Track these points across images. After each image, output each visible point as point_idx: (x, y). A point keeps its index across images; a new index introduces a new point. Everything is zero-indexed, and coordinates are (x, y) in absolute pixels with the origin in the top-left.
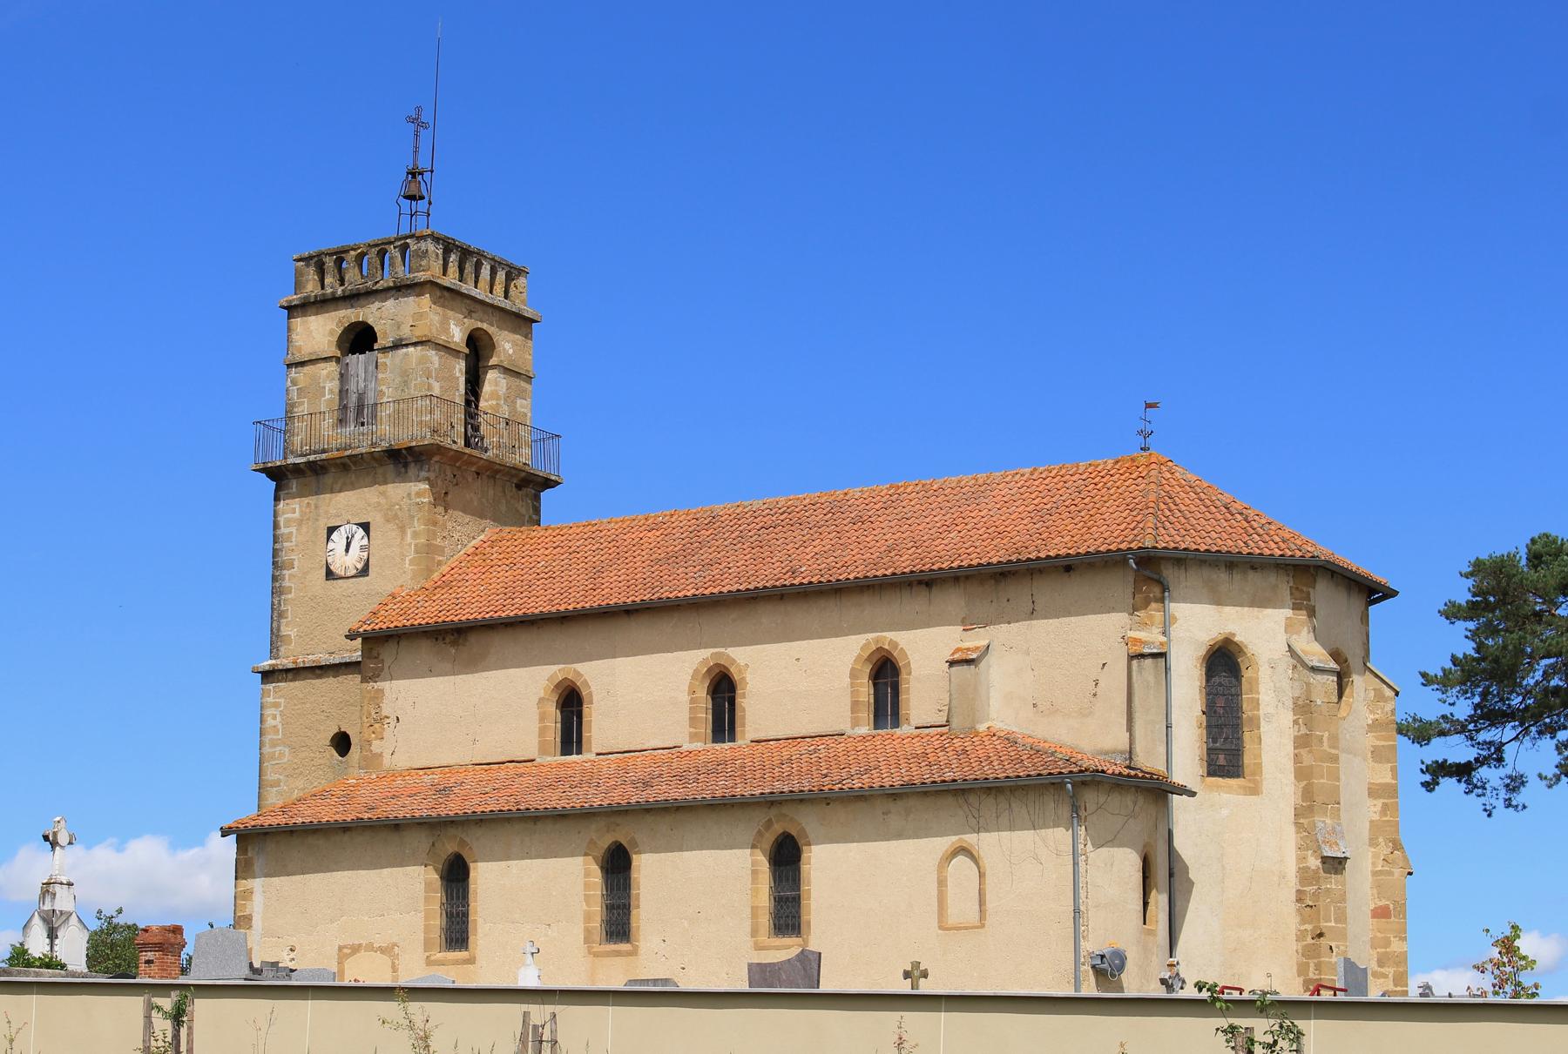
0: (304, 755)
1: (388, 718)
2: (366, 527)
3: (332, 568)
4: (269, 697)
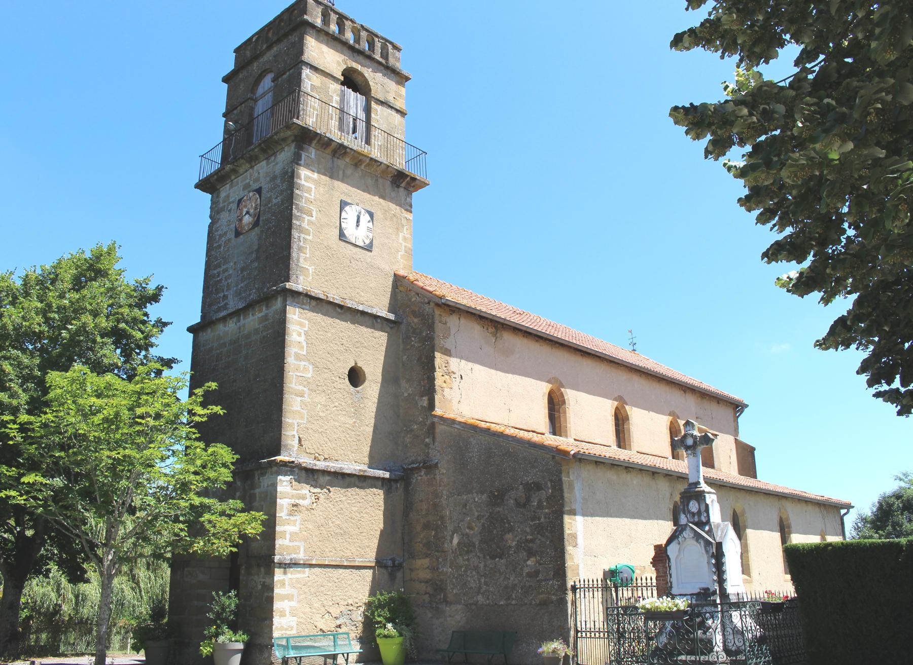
0: (325, 376)
1: (454, 373)
2: (371, 215)
3: (345, 232)
4: (295, 315)
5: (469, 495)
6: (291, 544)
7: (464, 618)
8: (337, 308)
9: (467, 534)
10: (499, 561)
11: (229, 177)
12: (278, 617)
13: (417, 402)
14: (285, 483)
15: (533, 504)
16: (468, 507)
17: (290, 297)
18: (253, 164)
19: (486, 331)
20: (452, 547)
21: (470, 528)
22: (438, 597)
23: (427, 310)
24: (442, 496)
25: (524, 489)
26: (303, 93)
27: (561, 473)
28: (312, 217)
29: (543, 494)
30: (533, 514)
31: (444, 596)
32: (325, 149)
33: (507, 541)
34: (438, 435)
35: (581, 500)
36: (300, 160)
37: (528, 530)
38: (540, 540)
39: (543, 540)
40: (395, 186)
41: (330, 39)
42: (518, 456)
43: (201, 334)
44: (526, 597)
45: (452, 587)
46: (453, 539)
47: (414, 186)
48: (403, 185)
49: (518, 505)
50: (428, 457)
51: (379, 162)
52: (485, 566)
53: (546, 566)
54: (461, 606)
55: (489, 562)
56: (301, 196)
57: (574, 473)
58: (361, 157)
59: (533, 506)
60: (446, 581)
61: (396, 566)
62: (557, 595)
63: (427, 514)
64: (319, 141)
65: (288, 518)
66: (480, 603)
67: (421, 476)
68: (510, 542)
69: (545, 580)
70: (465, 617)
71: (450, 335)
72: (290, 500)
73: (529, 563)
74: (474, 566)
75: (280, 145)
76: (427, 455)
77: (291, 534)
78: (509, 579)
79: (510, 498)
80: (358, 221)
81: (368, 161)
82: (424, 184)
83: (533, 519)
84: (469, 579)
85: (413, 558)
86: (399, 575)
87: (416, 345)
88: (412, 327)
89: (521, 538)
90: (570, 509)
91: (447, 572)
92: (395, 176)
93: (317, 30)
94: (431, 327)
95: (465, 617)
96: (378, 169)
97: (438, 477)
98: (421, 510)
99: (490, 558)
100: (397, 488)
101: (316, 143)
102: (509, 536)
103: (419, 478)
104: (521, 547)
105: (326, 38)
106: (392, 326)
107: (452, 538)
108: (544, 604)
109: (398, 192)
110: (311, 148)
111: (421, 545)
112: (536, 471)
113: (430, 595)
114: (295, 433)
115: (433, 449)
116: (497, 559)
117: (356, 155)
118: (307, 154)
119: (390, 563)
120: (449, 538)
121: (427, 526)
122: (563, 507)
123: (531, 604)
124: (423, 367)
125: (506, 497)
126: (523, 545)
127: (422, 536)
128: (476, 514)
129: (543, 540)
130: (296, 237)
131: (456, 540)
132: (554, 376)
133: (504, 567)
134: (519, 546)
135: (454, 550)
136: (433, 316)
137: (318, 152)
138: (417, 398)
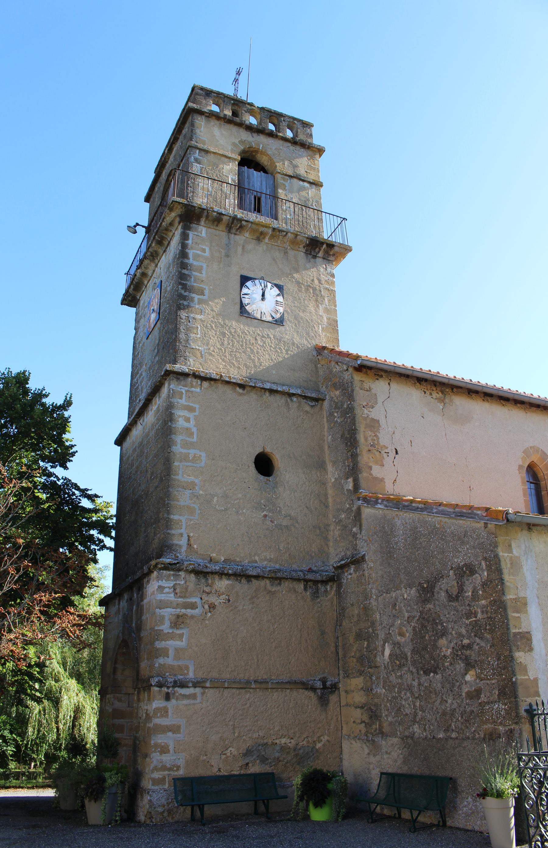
4: (181, 398)
5: (397, 592)
6: (176, 663)
7: (401, 756)
8: (238, 389)
9: (399, 643)
10: (434, 676)
11: (143, 283)
12: (158, 754)
13: (342, 486)
14: (167, 590)
15: (467, 594)
16: (397, 608)
17: (175, 380)
18: (156, 261)
19: (429, 397)
20: (384, 660)
21: (401, 634)
22: (374, 727)
23: (346, 378)
24: (371, 597)
25: (456, 575)
26: (192, 176)
27: (496, 546)
28: (204, 295)
29: (477, 579)
30: (468, 608)
31: (380, 725)
32: (217, 226)
33: (441, 649)
34: (364, 522)
35: (536, 584)
36: (188, 240)
37: (463, 631)
38: (478, 644)
39: (483, 644)
40: (310, 257)
41: (222, 123)
42: (446, 531)
43: (124, 445)
44: (467, 727)
45: (386, 713)
46: (384, 650)
47: (334, 255)
48: (321, 254)
49: (451, 598)
50: (356, 550)
51: (284, 231)
52: (420, 684)
53: (488, 682)
54: (397, 739)
55: (423, 678)
56: (189, 275)
57: (519, 547)
58: (262, 229)
59: (468, 597)
60: (381, 705)
61: (328, 688)
62: (505, 726)
63: (359, 620)
64: (207, 217)
65: (170, 631)
66: (417, 735)
67: (351, 574)
68: (444, 649)
69: (488, 703)
70: (401, 754)
71: (376, 403)
72: (174, 610)
73: (468, 678)
74: (408, 685)
75: (171, 231)
76: (355, 547)
77: (177, 650)
78: (447, 702)
79: (441, 589)
80: (263, 295)
81: (270, 231)
82: (347, 249)
83: (469, 615)
84: (404, 703)
85: (348, 677)
86: (333, 698)
87: (339, 421)
88: (334, 402)
89: (456, 644)
90: (514, 597)
91: (381, 694)
92: (307, 245)
93: (206, 116)
94: (351, 397)
95: (401, 754)
96: (286, 241)
97: (366, 573)
98: (353, 616)
99: (424, 672)
100: (326, 591)
101: (205, 221)
102: (443, 642)
103: (349, 577)
104: (457, 655)
105: (217, 122)
106: (313, 404)
107: (384, 650)
108: (492, 737)
109: (315, 262)
110: (200, 227)
111: (355, 660)
112: (467, 549)
113: (366, 724)
114: (182, 531)
115: (360, 539)
116: (432, 674)
117: (254, 226)
118: (196, 233)
119: (319, 684)
120: (380, 649)
121: (359, 636)
122: (503, 594)
123: (474, 739)
124: (347, 444)
125: (436, 589)
126: (460, 653)
127: (354, 649)
128: (406, 615)
129: (483, 644)
130: (184, 317)
131: (387, 652)
132: (532, 445)
133: (439, 685)
134: (455, 655)
135: (386, 665)
136: (351, 382)
137: (210, 230)
138: (343, 481)
